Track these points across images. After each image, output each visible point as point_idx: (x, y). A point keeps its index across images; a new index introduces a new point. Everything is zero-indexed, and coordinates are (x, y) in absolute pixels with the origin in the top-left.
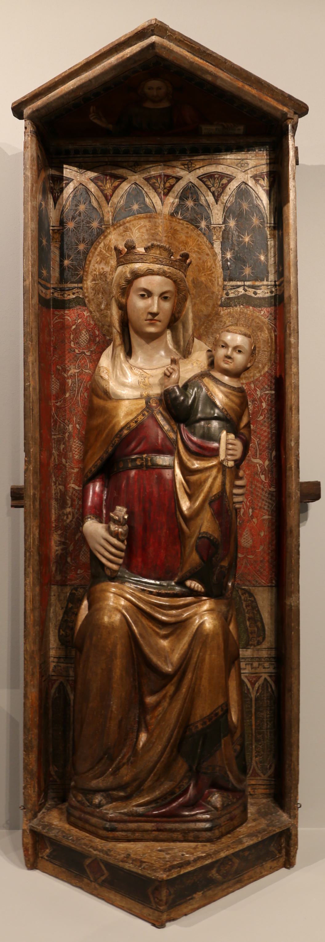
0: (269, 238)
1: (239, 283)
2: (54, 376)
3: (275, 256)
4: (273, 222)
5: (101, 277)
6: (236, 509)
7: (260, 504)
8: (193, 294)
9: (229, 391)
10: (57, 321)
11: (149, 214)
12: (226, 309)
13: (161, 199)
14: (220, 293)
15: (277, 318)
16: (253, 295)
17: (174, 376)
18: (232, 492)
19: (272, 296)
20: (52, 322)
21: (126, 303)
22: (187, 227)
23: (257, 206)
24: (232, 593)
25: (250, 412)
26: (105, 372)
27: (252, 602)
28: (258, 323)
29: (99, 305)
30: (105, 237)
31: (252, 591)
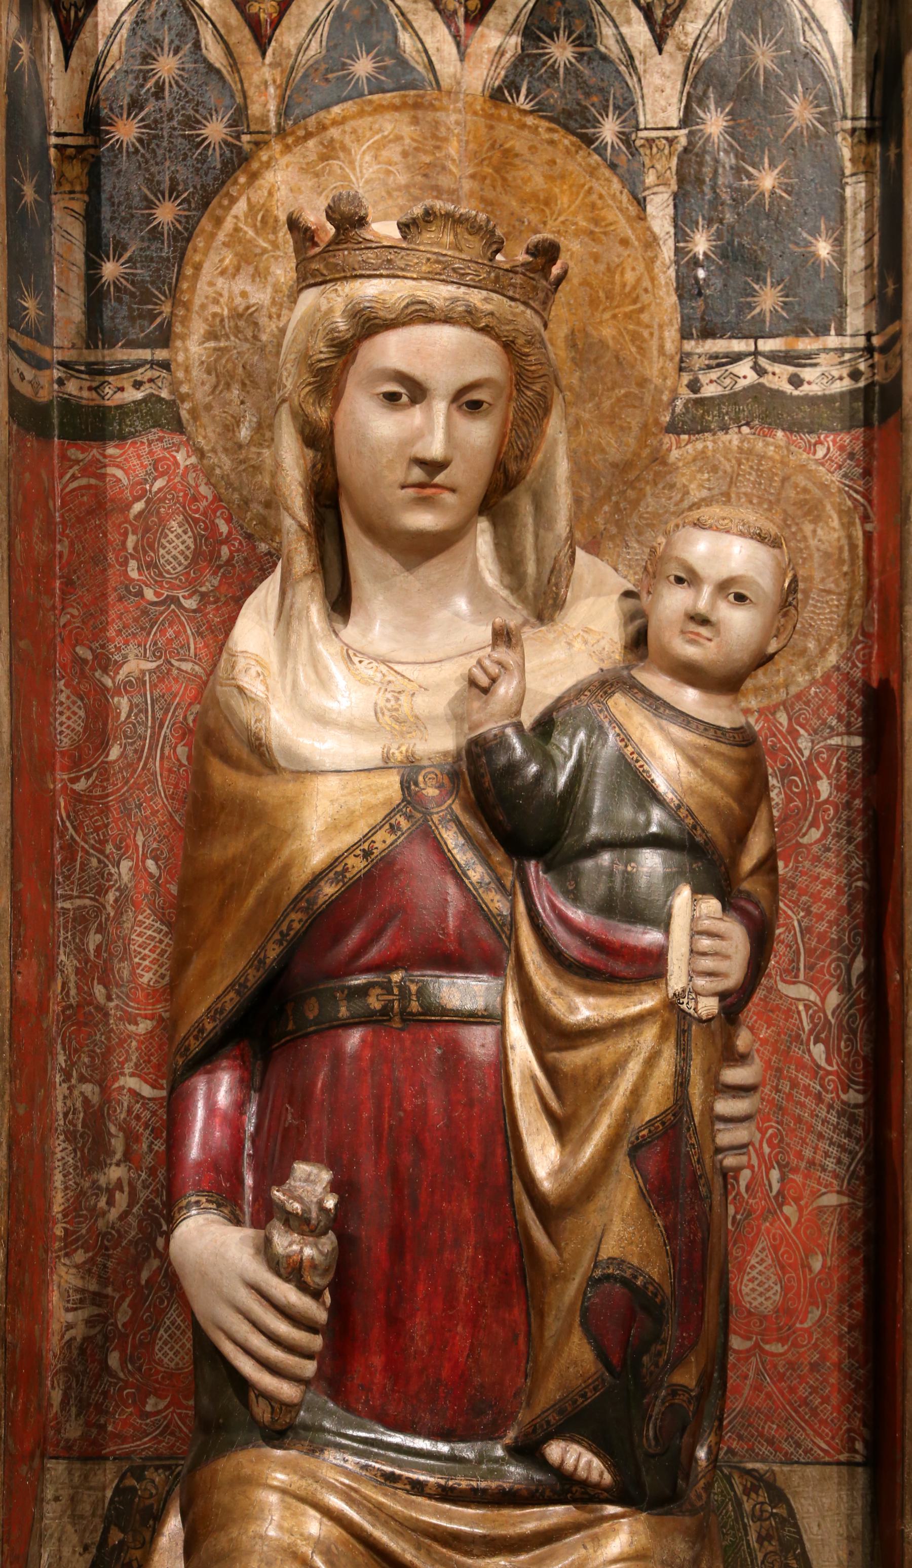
0: (848, 172)
1: (738, 346)
2: (67, 685)
3: (868, 241)
4: (863, 112)
5: (237, 326)
6: (725, 1173)
7: (808, 1153)
8: (571, 388)
9: (702, 741)
10: (75, 485)
11: (412, 92)
12: (689, 442)
13: (456, 37)
14: (669, 383)
15: (875, 473)
16: (788, 389)
17: (505, 690)
18: (712, 1109)
19: (859, 388)
20: (58, 487)
21: (332, 423)
22: (552, 142)
23: (806, 55)
24: (708, 1487)
25: (776, 813)
26: (253, 672)
27: (783, 1521)
28: (805, 490)
29: (230, 428)
30: (254, 176)
31: (780, 1483)
